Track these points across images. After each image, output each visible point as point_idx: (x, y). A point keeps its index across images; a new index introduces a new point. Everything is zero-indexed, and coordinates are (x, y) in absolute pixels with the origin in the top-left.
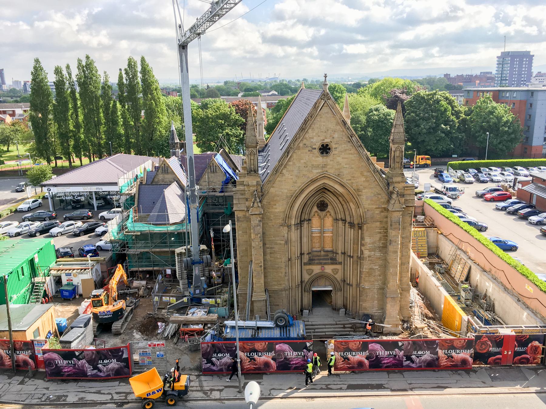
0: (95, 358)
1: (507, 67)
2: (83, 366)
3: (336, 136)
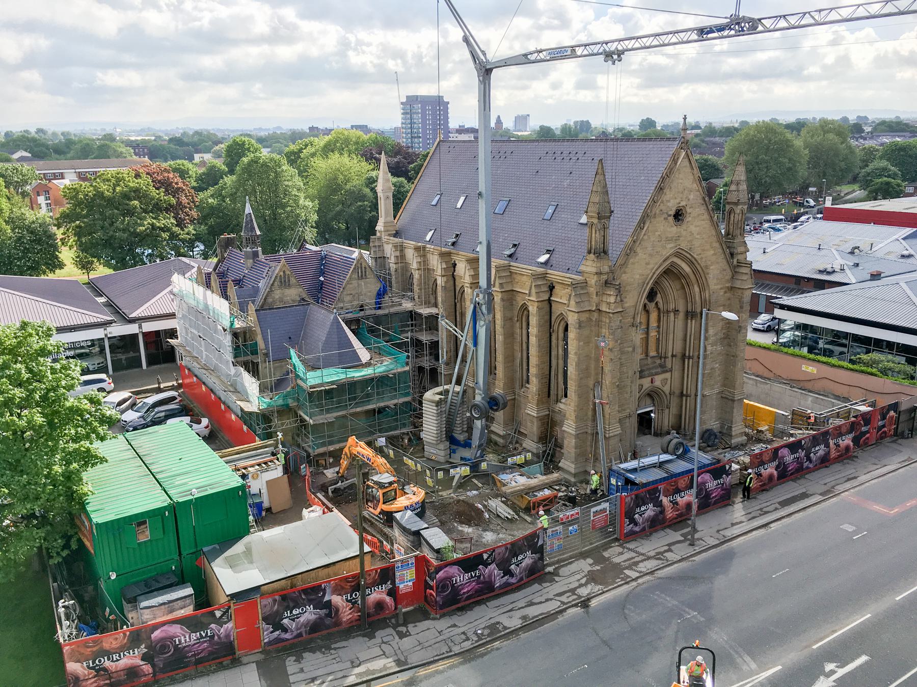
2: (490, 576)
3: (691, 197)
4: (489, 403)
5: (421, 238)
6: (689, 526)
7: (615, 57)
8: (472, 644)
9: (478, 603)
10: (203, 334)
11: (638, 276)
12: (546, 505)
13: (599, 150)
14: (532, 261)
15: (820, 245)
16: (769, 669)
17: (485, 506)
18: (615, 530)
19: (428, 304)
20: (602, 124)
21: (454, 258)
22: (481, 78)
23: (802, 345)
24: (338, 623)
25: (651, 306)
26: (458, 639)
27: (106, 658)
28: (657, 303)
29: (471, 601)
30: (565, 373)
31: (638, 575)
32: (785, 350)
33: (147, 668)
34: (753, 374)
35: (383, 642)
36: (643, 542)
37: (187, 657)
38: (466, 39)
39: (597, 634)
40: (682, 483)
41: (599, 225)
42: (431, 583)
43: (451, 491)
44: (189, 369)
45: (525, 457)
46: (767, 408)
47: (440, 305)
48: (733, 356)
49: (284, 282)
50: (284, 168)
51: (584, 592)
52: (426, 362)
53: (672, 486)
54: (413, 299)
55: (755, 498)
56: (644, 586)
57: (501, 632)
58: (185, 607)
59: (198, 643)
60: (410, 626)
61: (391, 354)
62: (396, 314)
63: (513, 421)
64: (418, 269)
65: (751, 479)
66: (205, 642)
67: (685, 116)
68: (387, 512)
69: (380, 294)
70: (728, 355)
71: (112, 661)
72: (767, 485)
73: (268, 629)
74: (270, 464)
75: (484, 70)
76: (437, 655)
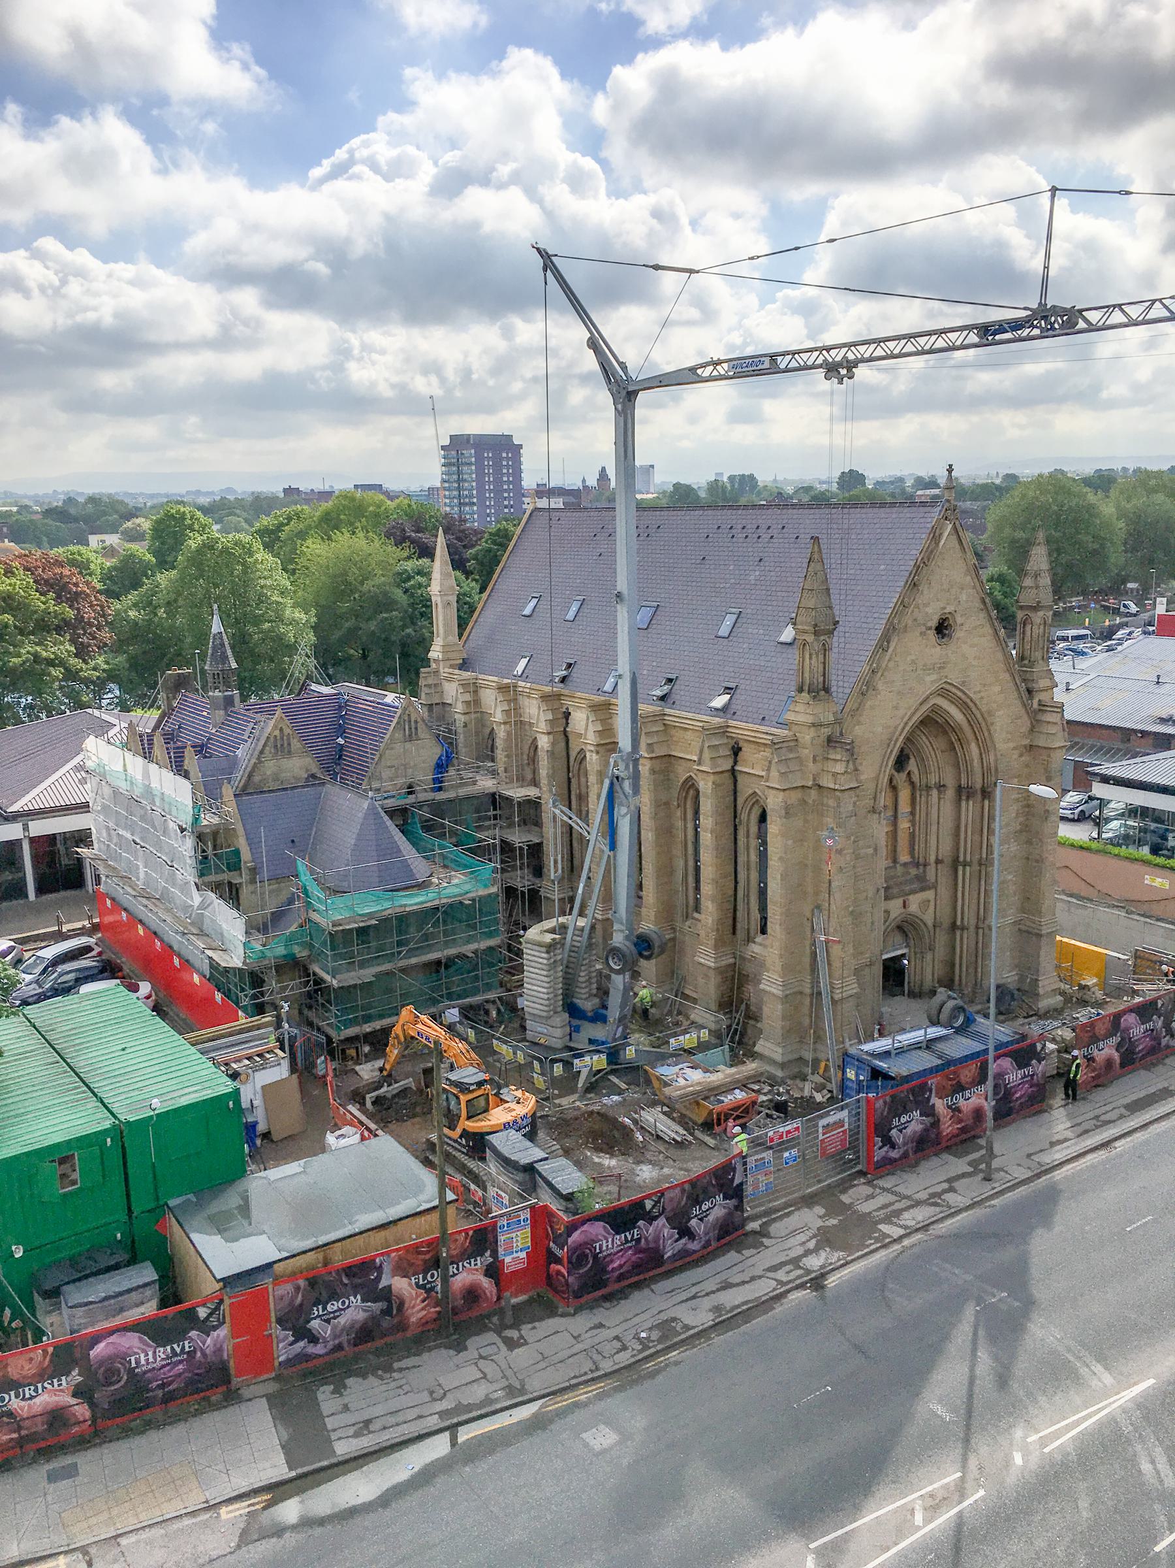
0: (301, 1305)
1: (470, 473)
2: (656, 1240)
3: (964, 597)
4: (635, 945)
5: (508, 671)
6: (981, 1147)
7: (843, 372)
8: (633, 1356)
9: (637, 1286)
10: (142, 839)
11: (880, 729)
12: (738, 1117)
13: (809, 522)
14: (701, 705)
15: (1158, 677)
16: (1135, 1384)
17: (635, 1122)
18: (858, 1157)
19: (521, 780)
20: (775, 480)
21: (568, 702)
22: (619, 407)
23: (1140, 843)
24: (402, 1326)
25: (900, 778)
26: (608, 1348)
27: (12, 1393)
28: (909, 773)
29: (627, 1282)
30: (763, 893)
31: (902, 1232)
32: (1116, 850)
33: (82, 1411)
34: (1064, 892)
35: (481, 1357)
36: (905, 1176)
37: (148, 1391)
38: (593, 343)
39: (843, 1334)
40: (967, 1074)
41: (815, 644)
42: (559, 1252)
43: (576, 1096)
44: (113, 899)
45: (699, 1037)
46: (1096, 949)
47: (544, 782)
48: (1037, 861)
49: (280, 747)
50: (259, 556)
51: (814, 1262)
52: (522, 880)
53: (951, 1079)
54: (494, 773)
55: (1084, 1099)
56: (915, 1250)
57: (680, 1334)
58: (143, 1303)
59: (168, 1364)
60: (526, 1329)
61: (466, 867)
62: (468, 798)
63: (673, 976)
64: (505, 723)
65: (1078, 1066)
66: (180, 1362)
67: (950, 466)
68: (475, 1134)
69: (441, 767)
70: (1028, 859)
71: (24, 1399)
72: (1104, 1076)
73: (286, 1337)
74: (268, 1056)
75: (624, 393)
76: (575, 1377)
